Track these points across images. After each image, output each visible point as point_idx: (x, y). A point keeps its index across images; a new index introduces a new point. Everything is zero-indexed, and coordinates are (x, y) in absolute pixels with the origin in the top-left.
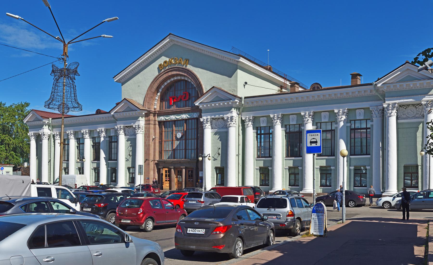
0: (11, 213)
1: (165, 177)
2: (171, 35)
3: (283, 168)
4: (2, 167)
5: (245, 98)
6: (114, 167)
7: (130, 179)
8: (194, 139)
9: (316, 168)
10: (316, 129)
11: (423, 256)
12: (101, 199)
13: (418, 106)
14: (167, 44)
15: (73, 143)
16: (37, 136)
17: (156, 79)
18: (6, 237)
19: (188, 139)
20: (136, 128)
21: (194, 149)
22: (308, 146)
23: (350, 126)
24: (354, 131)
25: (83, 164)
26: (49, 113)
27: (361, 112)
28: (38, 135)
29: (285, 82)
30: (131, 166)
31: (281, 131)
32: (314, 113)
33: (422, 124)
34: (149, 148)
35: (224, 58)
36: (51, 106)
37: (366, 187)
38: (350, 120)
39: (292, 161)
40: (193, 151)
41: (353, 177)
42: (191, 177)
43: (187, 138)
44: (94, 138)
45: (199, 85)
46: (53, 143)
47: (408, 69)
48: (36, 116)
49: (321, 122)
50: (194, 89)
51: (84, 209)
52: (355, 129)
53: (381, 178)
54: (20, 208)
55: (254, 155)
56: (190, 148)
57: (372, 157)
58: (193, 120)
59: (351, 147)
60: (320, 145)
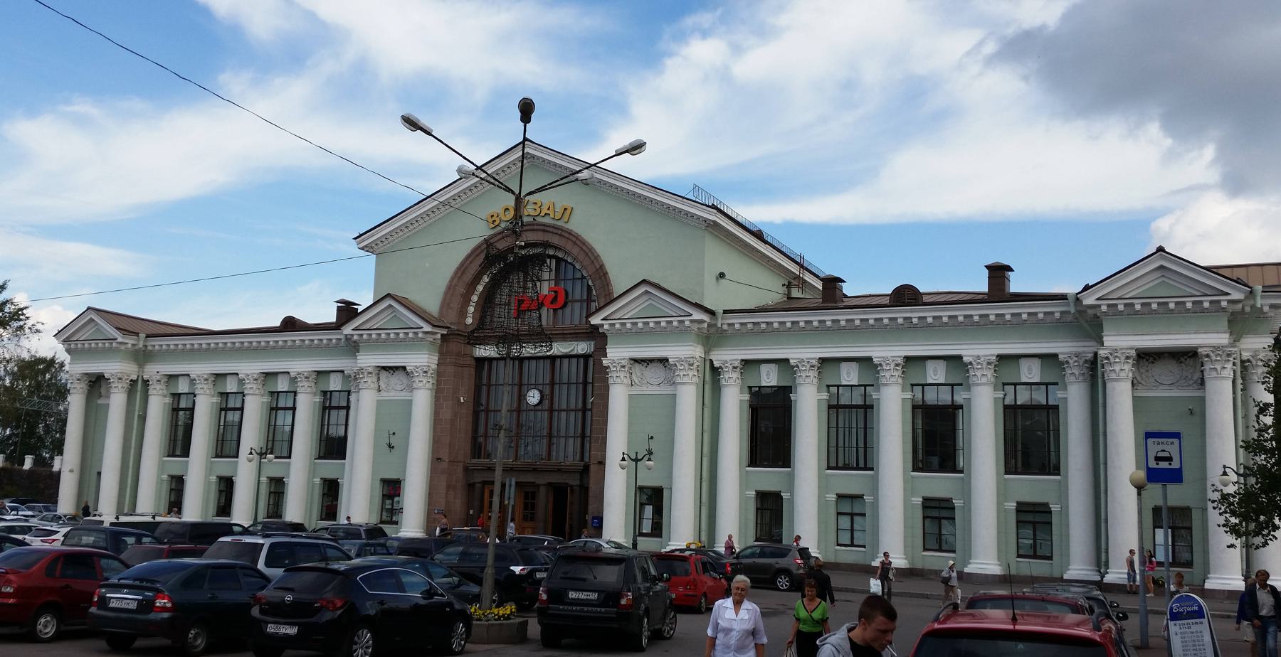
0: (779, 306)
1: (995, 391)
5: (726, 312)
6: (177, 472)
7: (324, 508)
8: (576, 410)
13: (1186, 357)
18: (63, 445)
20: (21, 317)
21: (567, 382)
22: (1150, 466)
24: (332, 405)
26: (111, 315)
28: (93, 380)
30: (800, 594)
31: (829, 270)
39: (1156, 530)
40: (573, 388)
41: (317, 501)
43: (556, 407)
44: (329, 393)
45: (601, 274)
48: (394, 311)
50: (578, 283)
53: (133, 445)
58: (574, 360)
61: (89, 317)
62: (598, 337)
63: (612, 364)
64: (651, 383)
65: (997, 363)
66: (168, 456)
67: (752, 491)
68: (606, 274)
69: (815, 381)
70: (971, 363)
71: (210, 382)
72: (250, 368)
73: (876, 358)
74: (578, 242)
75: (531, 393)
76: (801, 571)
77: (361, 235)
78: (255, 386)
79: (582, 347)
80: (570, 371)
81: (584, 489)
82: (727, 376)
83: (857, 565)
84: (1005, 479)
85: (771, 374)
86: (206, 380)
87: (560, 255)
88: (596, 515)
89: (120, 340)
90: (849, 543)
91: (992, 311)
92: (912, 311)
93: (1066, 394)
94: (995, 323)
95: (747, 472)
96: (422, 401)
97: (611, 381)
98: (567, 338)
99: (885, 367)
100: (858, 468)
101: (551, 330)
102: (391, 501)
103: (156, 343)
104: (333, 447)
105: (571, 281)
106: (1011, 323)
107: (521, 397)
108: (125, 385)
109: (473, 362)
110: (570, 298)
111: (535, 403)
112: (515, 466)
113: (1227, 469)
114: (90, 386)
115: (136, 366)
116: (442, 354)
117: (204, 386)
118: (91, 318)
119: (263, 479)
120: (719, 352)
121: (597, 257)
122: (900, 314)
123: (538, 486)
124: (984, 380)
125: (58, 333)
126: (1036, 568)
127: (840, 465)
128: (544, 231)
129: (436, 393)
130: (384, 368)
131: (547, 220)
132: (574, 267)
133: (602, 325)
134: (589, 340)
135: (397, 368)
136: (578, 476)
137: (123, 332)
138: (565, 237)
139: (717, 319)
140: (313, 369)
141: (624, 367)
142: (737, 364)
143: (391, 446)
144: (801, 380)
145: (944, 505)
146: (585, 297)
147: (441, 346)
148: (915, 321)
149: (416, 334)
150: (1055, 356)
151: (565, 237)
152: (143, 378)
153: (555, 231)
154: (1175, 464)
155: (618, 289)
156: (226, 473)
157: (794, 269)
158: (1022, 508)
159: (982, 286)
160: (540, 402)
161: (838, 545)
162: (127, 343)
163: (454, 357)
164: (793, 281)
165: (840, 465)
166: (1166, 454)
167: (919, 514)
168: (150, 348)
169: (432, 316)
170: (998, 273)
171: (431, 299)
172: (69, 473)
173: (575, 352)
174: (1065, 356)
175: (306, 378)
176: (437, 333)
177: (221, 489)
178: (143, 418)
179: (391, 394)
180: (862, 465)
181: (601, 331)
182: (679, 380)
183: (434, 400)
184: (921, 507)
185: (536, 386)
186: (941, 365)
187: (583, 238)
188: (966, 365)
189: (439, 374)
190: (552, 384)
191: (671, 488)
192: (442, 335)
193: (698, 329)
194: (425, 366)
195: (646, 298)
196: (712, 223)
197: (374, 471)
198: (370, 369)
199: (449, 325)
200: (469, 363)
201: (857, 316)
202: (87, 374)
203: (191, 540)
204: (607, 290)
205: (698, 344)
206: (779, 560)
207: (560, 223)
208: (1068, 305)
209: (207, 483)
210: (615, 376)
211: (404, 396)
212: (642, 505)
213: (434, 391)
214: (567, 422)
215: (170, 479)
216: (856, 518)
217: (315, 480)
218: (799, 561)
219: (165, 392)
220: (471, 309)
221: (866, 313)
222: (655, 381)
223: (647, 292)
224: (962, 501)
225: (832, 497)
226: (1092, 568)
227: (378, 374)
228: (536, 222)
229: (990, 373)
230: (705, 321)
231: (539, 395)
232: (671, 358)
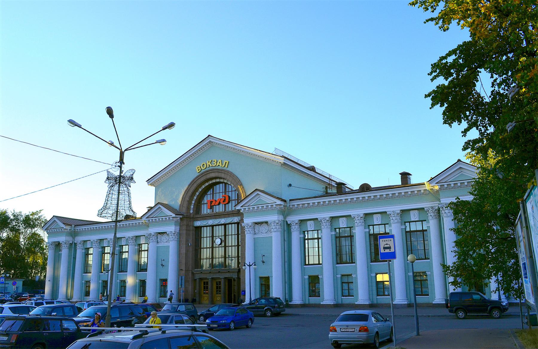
2: (210, 137)
3: (357, 283)
5: (290, 200)
8: (235, 246)
10: (469, 290)
11: (497, 299)
14: (205, 145)
16: (57, 245)
19: (228, 246)
23: (405, 229)
26: (62, 218)
29: (330, 183)
32: (365, 215)
35: (228, 176)
36: (103, 215)
38: (368, 225)
43: (227, 245)
47: (461, 168)
51: (468, 314)
52: (410, 232)
54: (343, 198)
56: (347, 247)
57: (356, 265)
58: (209, 227)
60: (380, 240)
71: (98, 243)
77: (149, 180)
79: (236, 219)
81: (239, 278)
87: (225, 181)
91: (403, 191)
105: (231, 192)
109: (194, 229)
110: (231, 199)
117: (96, 244)
120: (79, 238)
125: (431, 180)
126: (314, 300)
130: (159, 233)
134: (238, 216)
135: (164, 233)
136: (236, 274)
137: (66, 225)
143: (263, 262)
147: (180, 223)
152: (74, 243)
154: (392, 250)
157: (327, 181)
159: (398, 181)
160: (221, 244)
164: (328, 186)
166: (388, 246)
168: (76, 230)
170: (405, 176)
174: (427, 208)
175: (132, 239)
181: (241, 212)
189: (180, 234)
190: (225, 235)
192: (180, 218)
195: (459, 171)
199: (183, 214)
203: (524, 267)
219: (83, 247)
220: (192, 207)
232: (269, 221)
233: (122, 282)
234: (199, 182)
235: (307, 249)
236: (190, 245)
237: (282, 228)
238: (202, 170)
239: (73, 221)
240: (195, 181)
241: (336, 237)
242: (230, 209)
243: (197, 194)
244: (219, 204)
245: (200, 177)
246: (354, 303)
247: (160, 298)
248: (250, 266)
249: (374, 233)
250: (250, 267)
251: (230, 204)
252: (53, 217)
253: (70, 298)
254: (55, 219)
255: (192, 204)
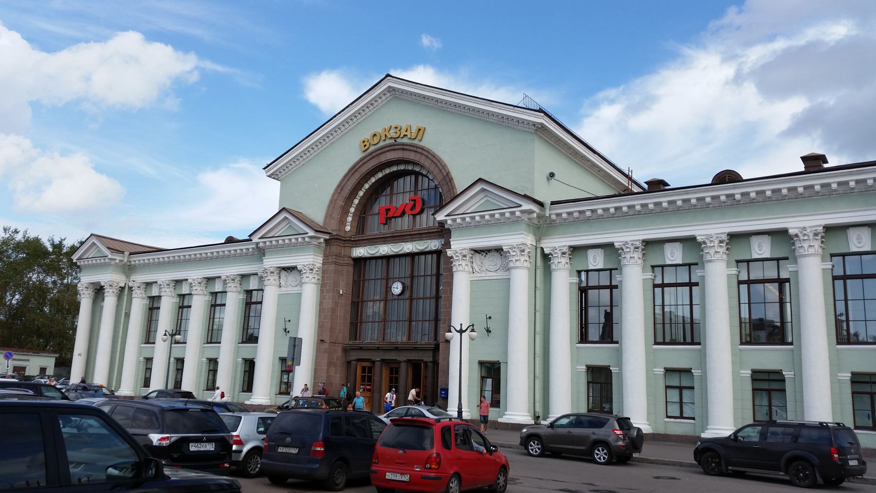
2: (389, 78)
4: (8, 353)
5: (553, 203)
8: (430, 298)
9: (221, 398)
12: (265, 427)
15: (199, 304)
17: (354, 170)
25: (211, 318)
27: (669, 257)
29: (630, 187)
32: (825, 229)
33: (108, 434)
34: (319, 313)
37: (793, 345)
42: (395, 383)
45: (448, 179)
46: (596, 155)
48: (289, 223)
49: (844, 250)
55: (848, 310)
58: (429, 256)
59: (767, 374)
61: (92, 242)
62: (443, 232)
63: (455, 254)
64: (489, 268)
65: (824, 234)
66: (145, 343)
67: (661, 368)
68: (451, 180)
69: (640, 262)
70: (797, 236)
72: (195, 274)
73: (547, 248)
74: (429, 156)
75: (395, 285)
76: (620, 443)
78: (199, 288)
79: (434, 244)
80: (426, 265)
81: (436, 363)
82: (556, 262)
83: (686, 436)
84: (837, 350)
85: (598, 258)
86: (168, 285)
87: (417, 169)
88: (443, 387)
89: (110, 256)
90: (678, 414)
92: (734, 188)
93: (621, 277)
94: (820, 194)
95: (577, 348)
96: (310, 293)
97: (454, 269)
98: (423, 237)
99: (709, 244)
100: (685, 343)
101: (410, 232)
102: (287, 376)
103: (137, 259)
104: (250, 338)
106: (802, 196)
107: (388, 289)
108: (115, 291)
109: (352, 262)
111: (398, 293)
112: (380, 346)
113: (167, 333)
114: (96, 293)
115: (124, 277)
116: (326, 256)
118: (93, 242)
119: (172, 359)
121: (444, 166)
122: (723, 191)
123: (400, 362)
124: (811, 251)
127: (667, 340)
128: (403, 149)
129: (321, 287)
130: (285, 269)
131: (405, 140)
132: (428, 178)
133: (446, 221)
136: (431, 354)
138: (420, 153)
139: (544, 210)
140: (204, 276)
141: (465, 256)
142: (565, 249)
143: (488, 331)
144: (625, 261)
145: (772, 377)
146: (438, 203)
147: (326, 249)
148: (738, 197)
149: (303, 238)
150: (611, 245)
151: (420, 153)
153: (411, 148)
155: (459, 189)
156: (212, 356)
158: (758, 376)
160: (402, 293)
161: (668, 417)
162: (115, 259)
163: (334, 257)
165: (668, 340)
167: (848, 390)
169: (319, 225)
171: (317, 213)
172: (79, 357)
173: (402, 252)
176: (320, 238)
177: (178, 368)
178: (128, 315)
179: (289, 289)
180: (689, 340)
181: (446, 227)
182: (511, 265)
183: (319, 293)
184: (849, 382)
185: (399, 279)
186: (766, 241)
187: (433, 152)
188: (700, 244)
190: (412, 277)
191: (507, 362)
192: (326, 240)
193: (529, 219)
194: (310, 264)
195: (482, 195)
196: (540, 126)
197: (275, 352)
198: (272, 270)
199: (331, 232)
200: (346, 262)
201: (678, 198)
202: (92, 283)
204: (452, 193)
205: (529, 233)
206: (596, 430)
207: (416, 142)
208: (124, 257)
209: (574, 374)
210: (457, 264)
211: (296, 290)
212: (483, 378)
213: (320, 286)
214: (424, 308)
215: (208, 362)
216: (685, 392)
217: (238, 360)
218: (618, 432)
220: (350, 219)
221: (687, 193)
222: (493, 268)
223: (483, 190)
224: (793, 373)
225: (660, 371)
226: (527, 414)
227: (280, 274)
228: (397, 143)
229: (817, 244)
230: (534, 212)
231: (401, 286)
233: (212, 362)
234: (364, 169)
235: (682, 325)
236: (341, 293)
237: (533, 260)
238: (371, 146)
239: (130, 247)
240: (356, 167)
241: (835, 278)
242: (424, 226)
243: (361, 193)
244: (403, 214)
245: (366, 160)
246: (697, 435)
247: (277, 396)
248: (461, 332)
249: (663, 281)
250: (461, 335)
251: (424, 216)
252: (91, 235)
253: (115, 389)
254: (94, 240)
255: (350, 214)
